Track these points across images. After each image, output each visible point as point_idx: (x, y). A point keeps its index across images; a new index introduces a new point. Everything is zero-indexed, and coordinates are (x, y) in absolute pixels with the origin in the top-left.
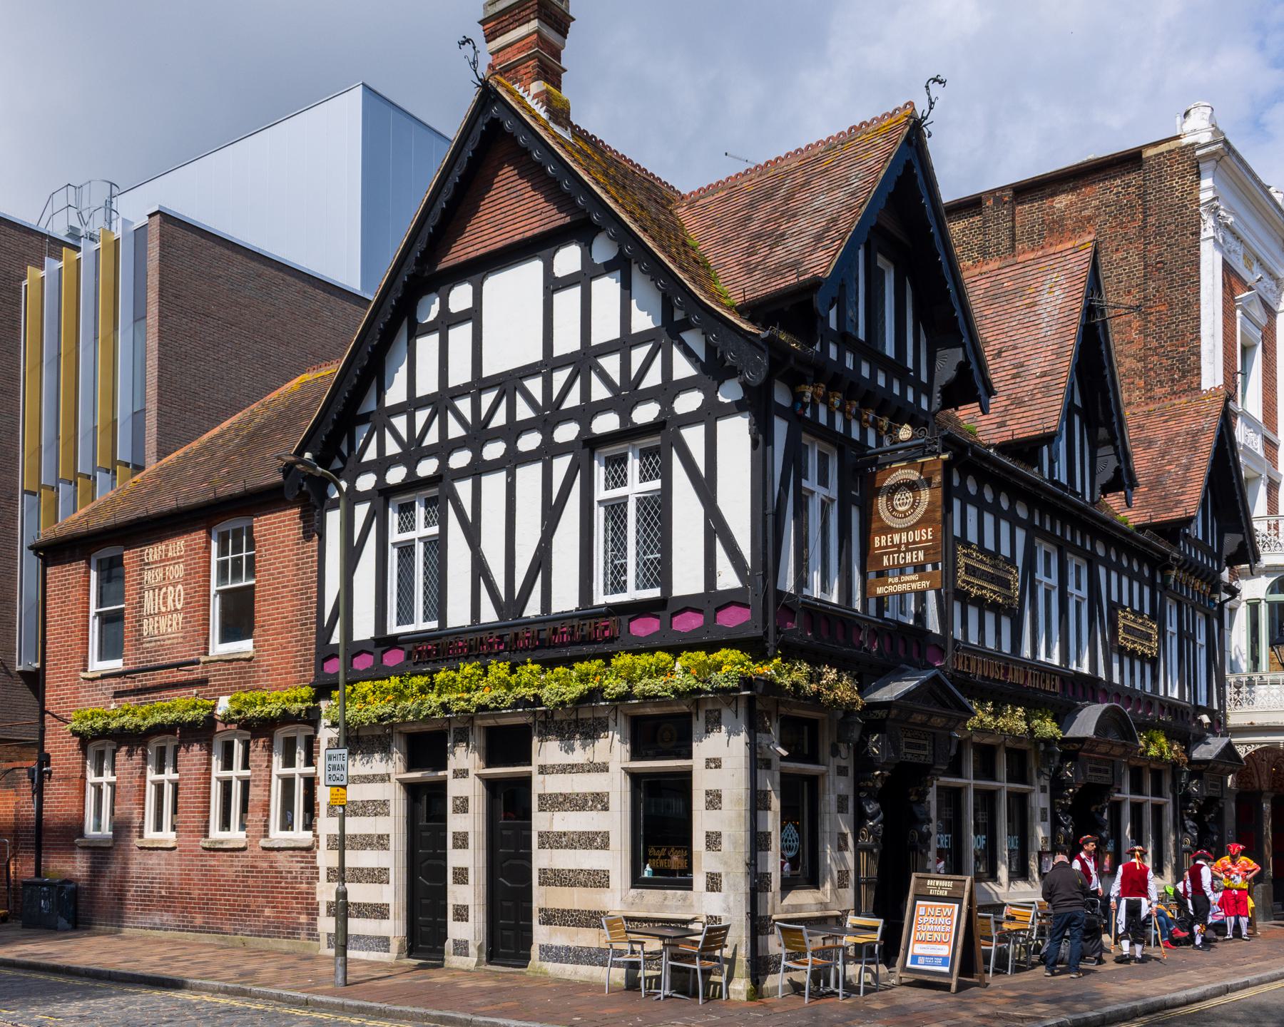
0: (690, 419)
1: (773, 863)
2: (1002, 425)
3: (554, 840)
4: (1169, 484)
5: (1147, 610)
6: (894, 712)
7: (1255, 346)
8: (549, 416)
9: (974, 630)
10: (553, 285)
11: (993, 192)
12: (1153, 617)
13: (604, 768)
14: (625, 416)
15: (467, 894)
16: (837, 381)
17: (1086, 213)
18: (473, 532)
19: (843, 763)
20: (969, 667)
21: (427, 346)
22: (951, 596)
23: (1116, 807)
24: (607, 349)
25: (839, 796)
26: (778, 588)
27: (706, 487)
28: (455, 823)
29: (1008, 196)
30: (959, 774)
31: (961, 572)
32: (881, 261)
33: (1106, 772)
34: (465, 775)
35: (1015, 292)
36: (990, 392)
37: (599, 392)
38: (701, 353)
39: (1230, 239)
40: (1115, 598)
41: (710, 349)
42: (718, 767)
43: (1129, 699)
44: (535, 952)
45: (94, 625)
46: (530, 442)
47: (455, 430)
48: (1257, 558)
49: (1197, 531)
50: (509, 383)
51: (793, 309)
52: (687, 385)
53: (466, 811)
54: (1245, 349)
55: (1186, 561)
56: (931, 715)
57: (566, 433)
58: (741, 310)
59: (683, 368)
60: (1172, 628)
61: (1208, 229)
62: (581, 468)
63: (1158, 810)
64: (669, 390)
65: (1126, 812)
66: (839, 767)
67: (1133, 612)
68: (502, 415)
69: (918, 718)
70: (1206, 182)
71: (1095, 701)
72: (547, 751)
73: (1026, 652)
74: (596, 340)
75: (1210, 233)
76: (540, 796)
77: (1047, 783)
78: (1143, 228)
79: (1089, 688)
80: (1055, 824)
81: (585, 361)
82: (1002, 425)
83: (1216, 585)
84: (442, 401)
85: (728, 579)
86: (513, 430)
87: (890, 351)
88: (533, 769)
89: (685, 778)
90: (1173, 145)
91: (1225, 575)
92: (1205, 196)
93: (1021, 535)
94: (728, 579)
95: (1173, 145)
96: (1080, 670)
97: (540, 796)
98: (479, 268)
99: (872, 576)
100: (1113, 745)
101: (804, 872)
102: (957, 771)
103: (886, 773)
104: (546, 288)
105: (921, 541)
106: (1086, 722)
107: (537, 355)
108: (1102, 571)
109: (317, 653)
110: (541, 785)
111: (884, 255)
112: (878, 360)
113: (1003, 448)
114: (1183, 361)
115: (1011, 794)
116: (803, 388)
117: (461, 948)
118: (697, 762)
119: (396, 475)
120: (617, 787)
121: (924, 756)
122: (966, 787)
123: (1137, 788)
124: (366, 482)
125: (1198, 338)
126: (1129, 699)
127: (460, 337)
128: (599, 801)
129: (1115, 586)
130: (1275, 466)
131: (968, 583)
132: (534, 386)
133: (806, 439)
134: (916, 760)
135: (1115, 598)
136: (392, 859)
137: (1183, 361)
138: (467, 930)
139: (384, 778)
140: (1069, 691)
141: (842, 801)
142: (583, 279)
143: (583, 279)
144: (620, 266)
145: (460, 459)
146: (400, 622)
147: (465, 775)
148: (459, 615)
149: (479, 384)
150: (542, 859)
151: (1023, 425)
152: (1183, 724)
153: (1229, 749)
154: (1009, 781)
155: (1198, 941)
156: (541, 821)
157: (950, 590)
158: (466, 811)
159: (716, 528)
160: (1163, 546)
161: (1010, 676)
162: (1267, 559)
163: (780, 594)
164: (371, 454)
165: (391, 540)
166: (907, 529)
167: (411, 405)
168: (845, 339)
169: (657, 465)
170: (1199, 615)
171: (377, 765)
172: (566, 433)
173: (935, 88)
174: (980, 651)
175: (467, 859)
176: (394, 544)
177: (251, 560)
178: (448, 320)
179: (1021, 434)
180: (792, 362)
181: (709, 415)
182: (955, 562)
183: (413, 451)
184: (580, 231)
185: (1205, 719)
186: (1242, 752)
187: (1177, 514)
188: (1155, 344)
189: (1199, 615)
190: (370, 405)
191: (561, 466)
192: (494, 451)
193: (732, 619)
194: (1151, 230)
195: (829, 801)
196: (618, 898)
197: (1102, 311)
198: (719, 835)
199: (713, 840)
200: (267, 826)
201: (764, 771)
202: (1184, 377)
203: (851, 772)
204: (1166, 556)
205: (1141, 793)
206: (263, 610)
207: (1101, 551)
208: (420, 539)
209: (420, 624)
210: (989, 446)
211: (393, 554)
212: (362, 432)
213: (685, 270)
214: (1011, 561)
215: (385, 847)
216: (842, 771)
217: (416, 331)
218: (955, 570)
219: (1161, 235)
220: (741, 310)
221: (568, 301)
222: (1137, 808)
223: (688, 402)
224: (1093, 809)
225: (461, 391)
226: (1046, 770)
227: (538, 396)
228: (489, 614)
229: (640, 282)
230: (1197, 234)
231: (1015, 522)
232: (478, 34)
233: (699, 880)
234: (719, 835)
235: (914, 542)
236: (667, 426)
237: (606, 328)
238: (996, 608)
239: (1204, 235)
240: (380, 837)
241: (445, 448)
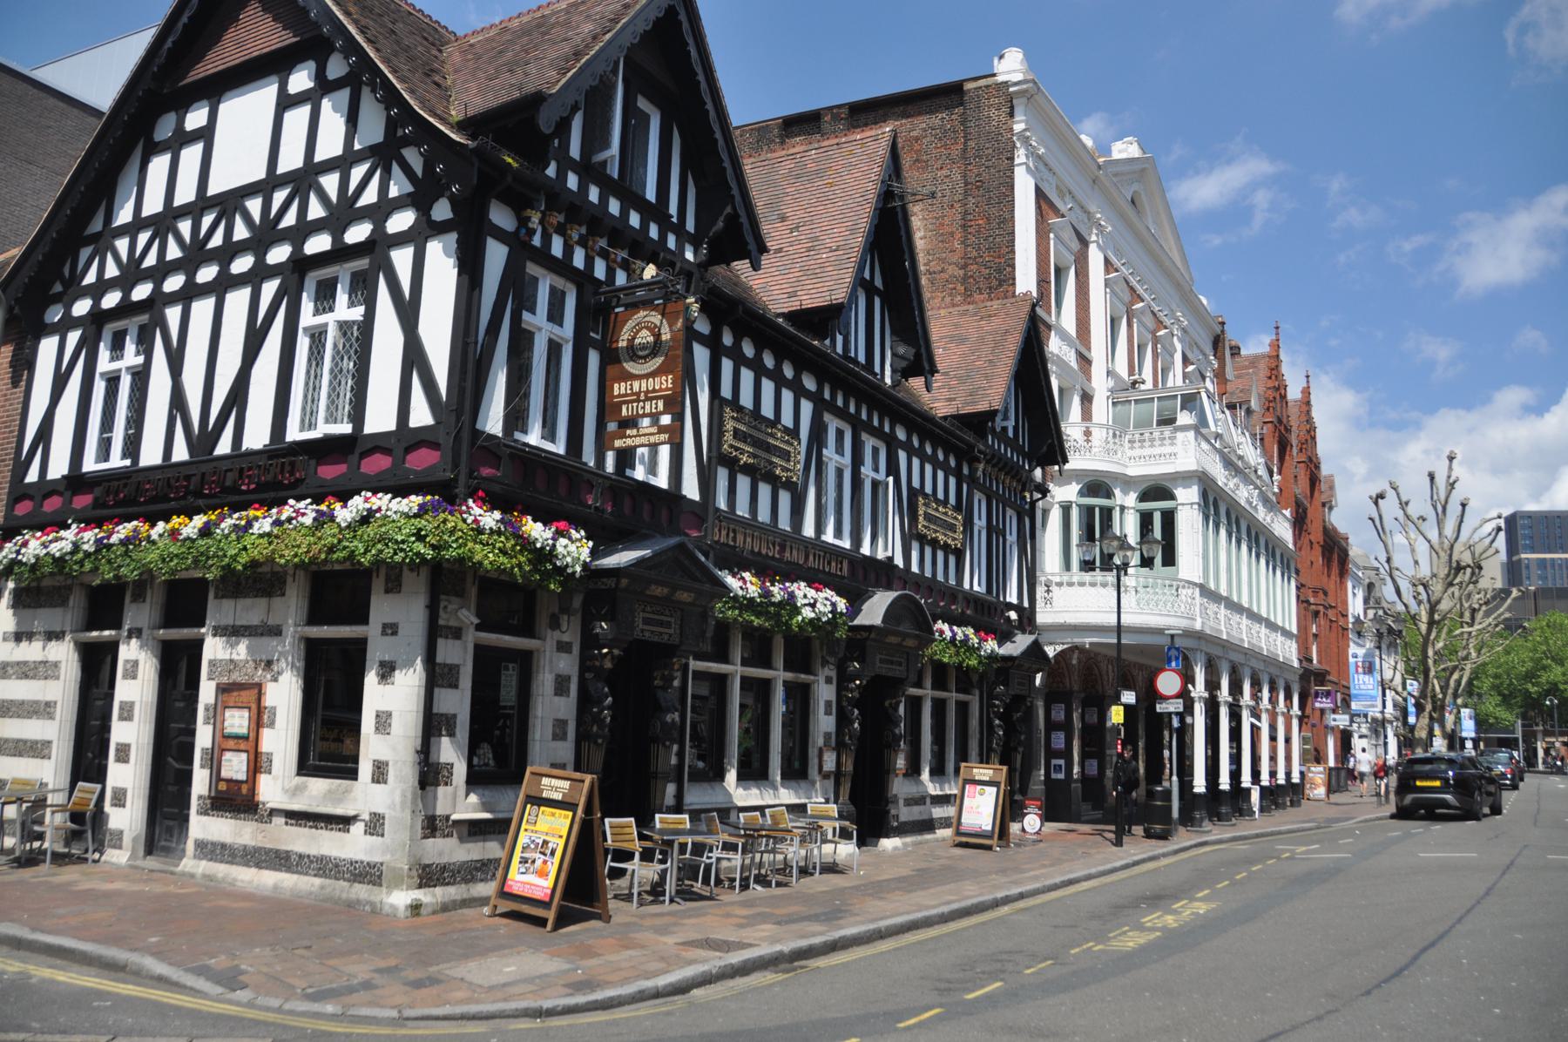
0: (401, 239)
2: (793, 295)
4: (965, 374)
5: (952, 500)
6: (624, 582)
7: (1068, 268)
8: (266, 235)
9: (741, 499)
10: (286, 102)
11: (830, 108)
12: (958, 508)
13: (276, 632)
14: (338, 237)
16: (574, 211)
17: (914, 134)
18: (176, 362)
19: (566, 638)
20: (734, 539)
21: (159, 166)
22: (714, 461)
24: (329, 166)
25: (558, 676)
26: (478, 426)
27: (408, 312)
29: (844, 112)
30: (725, 659)
31: (728, 437)
32: (643, 104)
33: (900, 664)
35: (817, 172)
36: (763, 249)
37: (112, 271)
38: (418, 169)
39: (1042, 167)
40: (916, 483)
41: (428, 166)
42: (395, 633)
43: (930, 589)
47: (316, 211)
48: (1065, 460)
49: (999, 423)
50: (230, 203)
51: (518, 126)
53: (134, 677)
54: (1058, 271)
55: (993, 456)
56: (674, 588)
57: (279, 254)
58: (461, 126)
60: (980, 523)
61: (1021, 156)
62: (290, 295)
63: (963, 708)
66: (559, 643)
67: (937, 501)
69: (659, 591)
70: (1019, 117)
71: (889, 587)
73: (809, 530)
74: (319, 157)
75: (1023, 159)
76: (210, 662)
77: (833, 674)
78: (964, 150)
79: (882, 574)
80: (843, 720)
81: (304, 180)
82: (793, 295)
83: (1026, 483)
84: (163, 224)
85: (421, 415)
86: (231, 250)
87: (651, 194)
89: (360, 645)
90: (989, 81)
91: (1038, 473)
92: (1018, 127)
93: (807, 407)
95: (989, 81)
96: (654, 481)
97: (210, 662)
98: (218, 88)
99: (612, 427)
100: (905, 636)
102: (919, 685)
103: (616, 652)
104: (278, 104)
105: (661, 390)
106: (875, 610)
107: (260, 173)
108: (902, 455)
109: (9, 493)
111: (645, 95)
112: (633, 199)
113: (791, 316)
114: (999, 271)
115: (745, 680)
116: (529, 212)
118: (372, 631)
119: (319, 244)
121: (897, 671)
122: (733, 675)
123: (939, 684)
124: (82, 307)
125: (1013, 252)
126: (930, 589)
127: (191, 155)
129: (915, 471)
130: (1089, 380)
131: (737, 449)
133: (827, 417)
134: (656, 639)
135: (916, 483)
137: (999, 271)
140: (859, 576)
144: (352, 82)
145: (174, 283)
146: (98, 460)
148: (151, 455)
149: (203, 203)
151: (813, 297)
152: (987, 614)
153: (1036, 650)
154: (743, 664)
155: (1541, 767)
157: (714, 454)
158: (134, 677)
159: (414, 357)
160: (969, 437)
161: (787, 554)
162: (1075, 463)
163: (477, 434)
164: (90, 278)
166: (647, 376)
167: (138, 224)
168: (590, 171)
169: (363, 290)
170: (1009, 512)
172: (279, 254)
174: (751, 524)
176: (102, 374)
178: (183, 138)
179: (809, 303)
180: (509, 179)
181: (417, 238)
182: (721, 423)
183: (132, 273)
185: (1013, 615)
186: (1051, 651)
187: (982, 406)
188: (975, 254)
189: (1009, 512)
190: (97, 225)
191: (270, 289)
192: (207, 274)
193: (422, 461)
194: (970, 154)
195: (544, 682)
197: (902, 198)
198: (389, 715)
199: (383, 722)
201: (450, 642)
202: (1000, 285)
203: (576, 649)
204: (972, 447)
205: (945, 689)
207: (901, 434)
208: (128, 369)
209: (117, 461)
210: (779, 315)
211: (99, 388)
212: (85, 253)
213: (402, 80)
214: (794, 432)
215: (51, 717)
216: (563, 647)
218: (721, 433)
219: (980, 157)
220: (461, 126)
221: (297, 119)
222: (939, 707)
223: (401, 221)
224: (887, 704)
226: (832, 660)
227: (256, 216)
228: (181, 453)
230: (1012, 159)
231: (800, 392)
233: (365, 769)
234: (389, 715)
235: (654, 391)
236: (378, 246)
237: (331, 144)
238: (748, 470)
239: (1017, 161)
240: (48, 704)
241: (164, 269)
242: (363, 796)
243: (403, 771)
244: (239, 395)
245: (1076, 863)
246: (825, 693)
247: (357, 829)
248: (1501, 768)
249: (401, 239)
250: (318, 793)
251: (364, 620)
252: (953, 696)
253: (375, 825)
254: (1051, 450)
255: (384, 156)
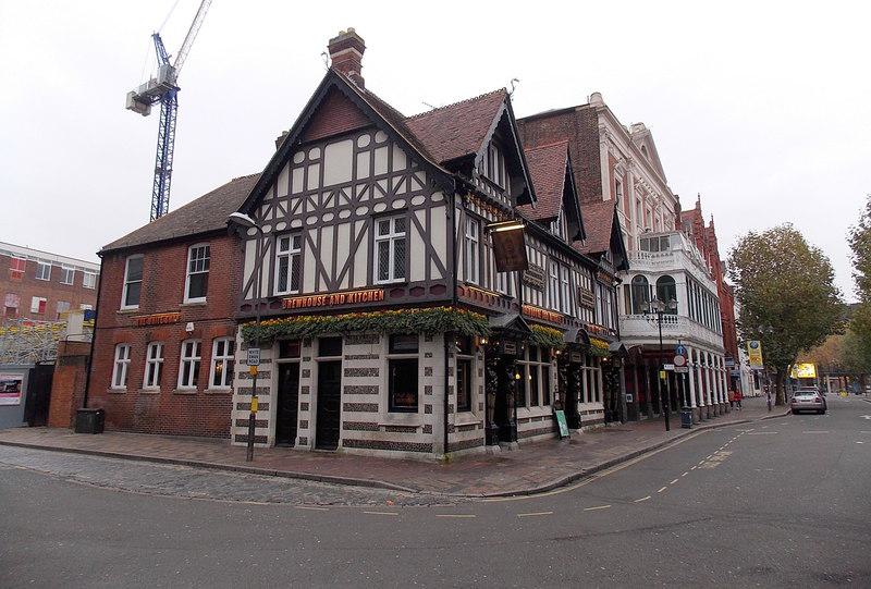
0: (419, 208)
1: (453, 400)
3: (351, 390)
4: (596, 239)
8: (354, 203)
10: (357, 151)
15: (307, 416)
18: (317, 253)
21: (298, 174)
23: (581, 371)
27: (426, 236)
28: (303, 382)
34: (309, 363)
44: (340, 442)
45: (125, 289)
46: (345, 214)
50: (337, 190)
52: (418, 193)
57: (362, 211)
58: (441, 164)
59: (415, 187)
62: (369, 227)
63: (596, 372)
64: (409, 195)
65: (585, 374)
68: (331, 205)
72: (347, 350)
76: (345, 370)
80: (488, 379)
81: (372, 182)
84: (305, 196)
86: (337, 209)
87: (497, 182)
88: (343, 357)
89: (415, 362)
94: (436, 275)
97: (345, 370)
101: (465, 405)
110: (345, 365)
112: (492, 185)
115: (543, 367)
117: (304, 441)
118: (421, 355)
120: (382, 365)
123: (533, 358)
127: (314, 170)
128: (374, 372)
132: (348, 191)
136: (270, 399)
138: (307, 433)
139: (269, 361)
141: (480, 370)
142: (372, 148)
143: (372, 148)
145: (312, 221)
147: (309, 363)
148: (417, 274)
149: (321, 191)
150: (345, 399)
156: (345, 381)
159: (430, 253)
165: (376, 239)
167: (290, 197)
171: (265, 354)
172: (362, 211)
173: (515, 83)
175: (308, 398)
177: (207, 262)
178: (307, 164)
181: (428, 206)
183: (290, 216)
184: (371, 129)
190: (270, 196)
191: (359, 225)
192: (328, 218)
196: (382, 416)
199: (428, 390)
200: (208, 383)
206: (212, 284)
217: (294, 166)
221: (364, 158)
223: (418, 201)
225: (314, 192)
228: (323, 288)
229: (395, 147)
232: (327, 51)
233: (421, 408)
237: (381, 168)
242: (421, 418)
243: (438, 409)
244: (350, 263)
245: (646, 440)
246: (554, 370)
247: (419, 431)
248: (64, 376)
249: (419, 208)
250: (400, 418)
251: (416, 351)
252: (592, 368)
253: (428, 429)
254: (624, 266)
255: (406, 175)
